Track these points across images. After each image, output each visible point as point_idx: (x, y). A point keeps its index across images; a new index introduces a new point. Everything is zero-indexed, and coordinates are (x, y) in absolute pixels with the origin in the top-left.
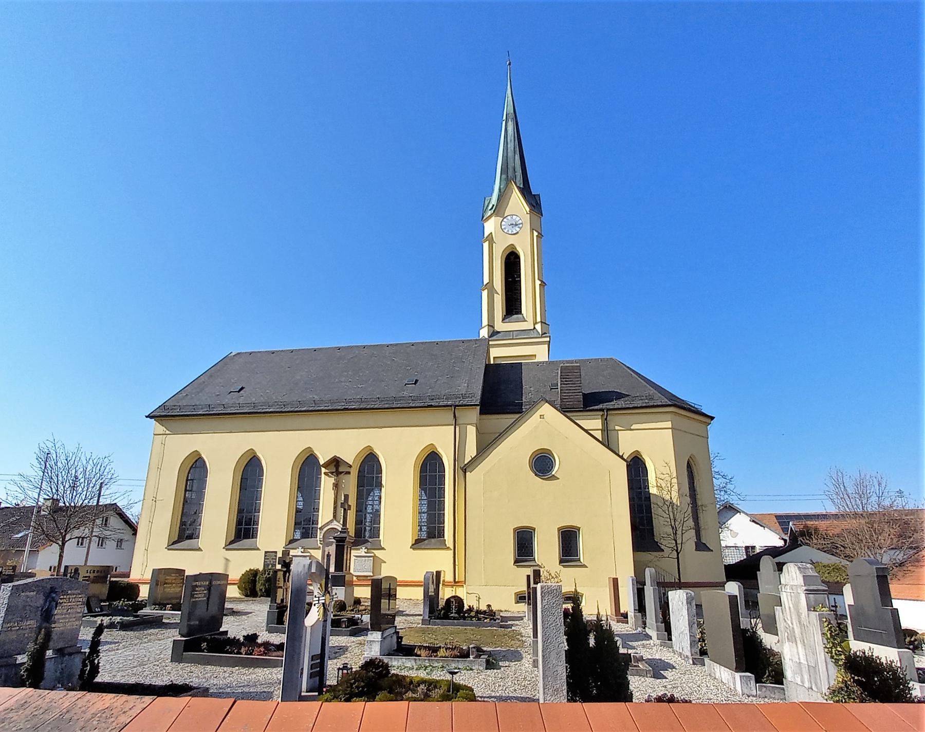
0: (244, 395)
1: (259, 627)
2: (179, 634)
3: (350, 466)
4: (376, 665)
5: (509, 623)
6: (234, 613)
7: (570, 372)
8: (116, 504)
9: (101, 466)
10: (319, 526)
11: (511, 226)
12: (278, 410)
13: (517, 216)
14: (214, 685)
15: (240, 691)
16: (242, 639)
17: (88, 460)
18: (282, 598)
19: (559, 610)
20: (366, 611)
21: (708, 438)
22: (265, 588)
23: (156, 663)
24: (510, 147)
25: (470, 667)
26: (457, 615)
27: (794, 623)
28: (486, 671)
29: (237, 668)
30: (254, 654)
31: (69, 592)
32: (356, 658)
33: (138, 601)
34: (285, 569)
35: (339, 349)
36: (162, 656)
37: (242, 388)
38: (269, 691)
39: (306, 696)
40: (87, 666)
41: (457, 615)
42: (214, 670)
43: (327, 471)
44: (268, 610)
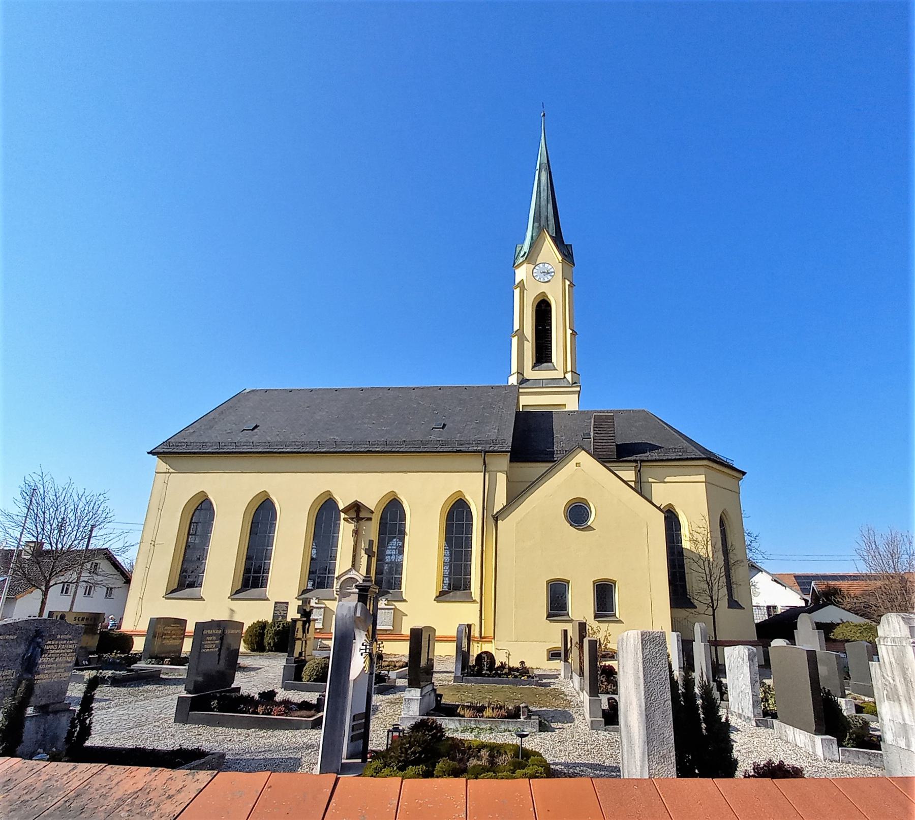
0: (259, 433)
1: (271, 684)
2: (185, 690)
3: (372, 512)
4: (429, 726)
5: (544, 681)
6: (244, 669)
7: (603, 422)
8: (107, 548)
9: (95, 504)
10: (336, 575)
11: (543, 274)
12: (295, 450)
13: (549, 264)
14: (229, 750)
15: (262, 757)
16: (257, 697)
17: (80, 497)
18: (300, 651)
19: (664, 660)
20: (391, 667)
21: (740, 493)
22: (274, 642)
23: (156, 724)
24: (543, 197)
25: (522, 729)
26: (488, 672)
27: (897, 680)
28: (539, 734)
29: (253, 730)
30: (272, 713)
31: (59, 637)
32: (389, 719)
33: (131, 654)
34: (305, 619)
35: (362, 390)
36: (162, 716)
37: (256, 427)
38: (296, 757)
39: (347, 763)
40: (77, 727)
41: (488, 672)
42: (226, 732)
43: (346, 516)
44: (285, 664)
